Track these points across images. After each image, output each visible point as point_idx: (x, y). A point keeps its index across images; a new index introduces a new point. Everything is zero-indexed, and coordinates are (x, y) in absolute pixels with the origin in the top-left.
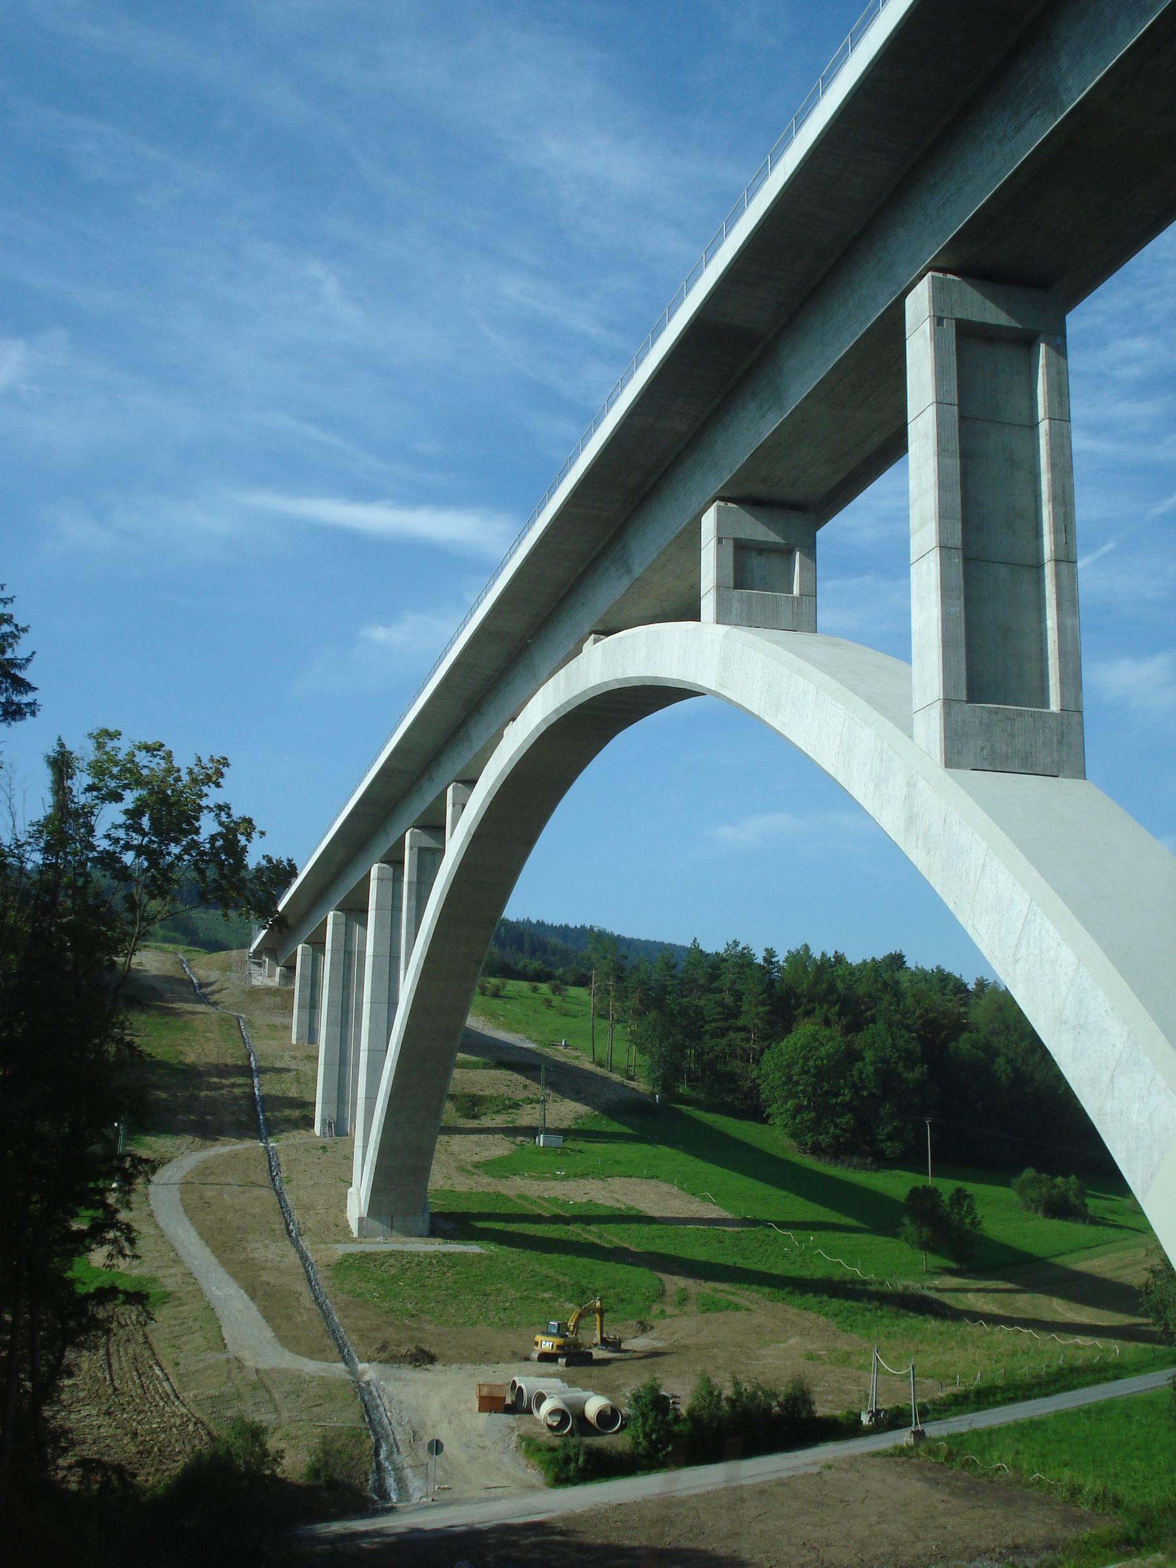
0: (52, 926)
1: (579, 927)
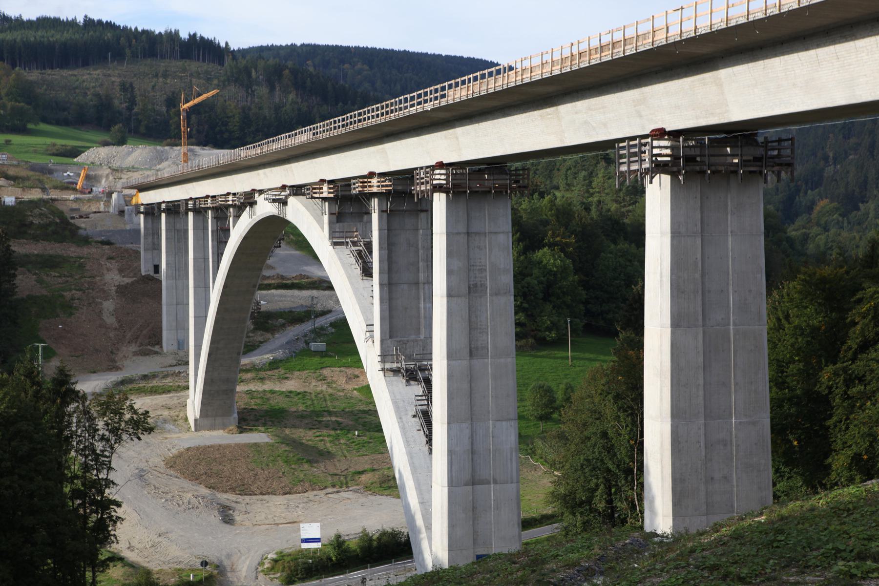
0: (101, 499)
1: (140, 29)
